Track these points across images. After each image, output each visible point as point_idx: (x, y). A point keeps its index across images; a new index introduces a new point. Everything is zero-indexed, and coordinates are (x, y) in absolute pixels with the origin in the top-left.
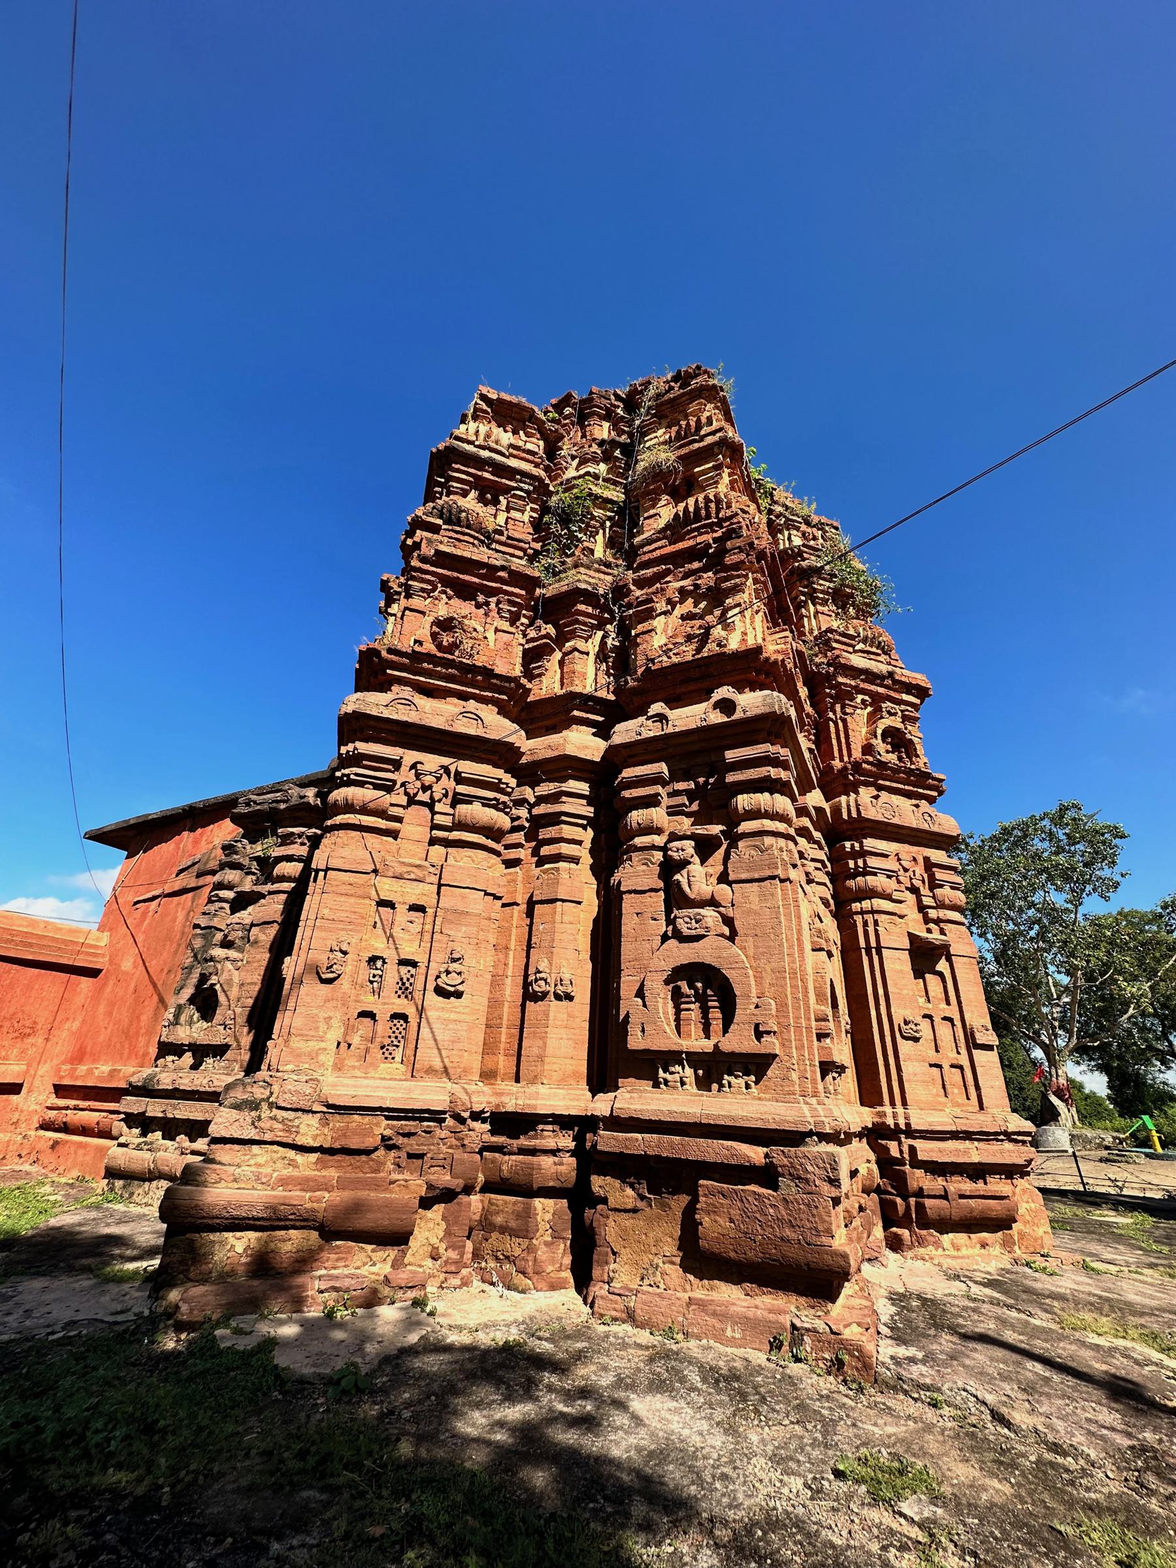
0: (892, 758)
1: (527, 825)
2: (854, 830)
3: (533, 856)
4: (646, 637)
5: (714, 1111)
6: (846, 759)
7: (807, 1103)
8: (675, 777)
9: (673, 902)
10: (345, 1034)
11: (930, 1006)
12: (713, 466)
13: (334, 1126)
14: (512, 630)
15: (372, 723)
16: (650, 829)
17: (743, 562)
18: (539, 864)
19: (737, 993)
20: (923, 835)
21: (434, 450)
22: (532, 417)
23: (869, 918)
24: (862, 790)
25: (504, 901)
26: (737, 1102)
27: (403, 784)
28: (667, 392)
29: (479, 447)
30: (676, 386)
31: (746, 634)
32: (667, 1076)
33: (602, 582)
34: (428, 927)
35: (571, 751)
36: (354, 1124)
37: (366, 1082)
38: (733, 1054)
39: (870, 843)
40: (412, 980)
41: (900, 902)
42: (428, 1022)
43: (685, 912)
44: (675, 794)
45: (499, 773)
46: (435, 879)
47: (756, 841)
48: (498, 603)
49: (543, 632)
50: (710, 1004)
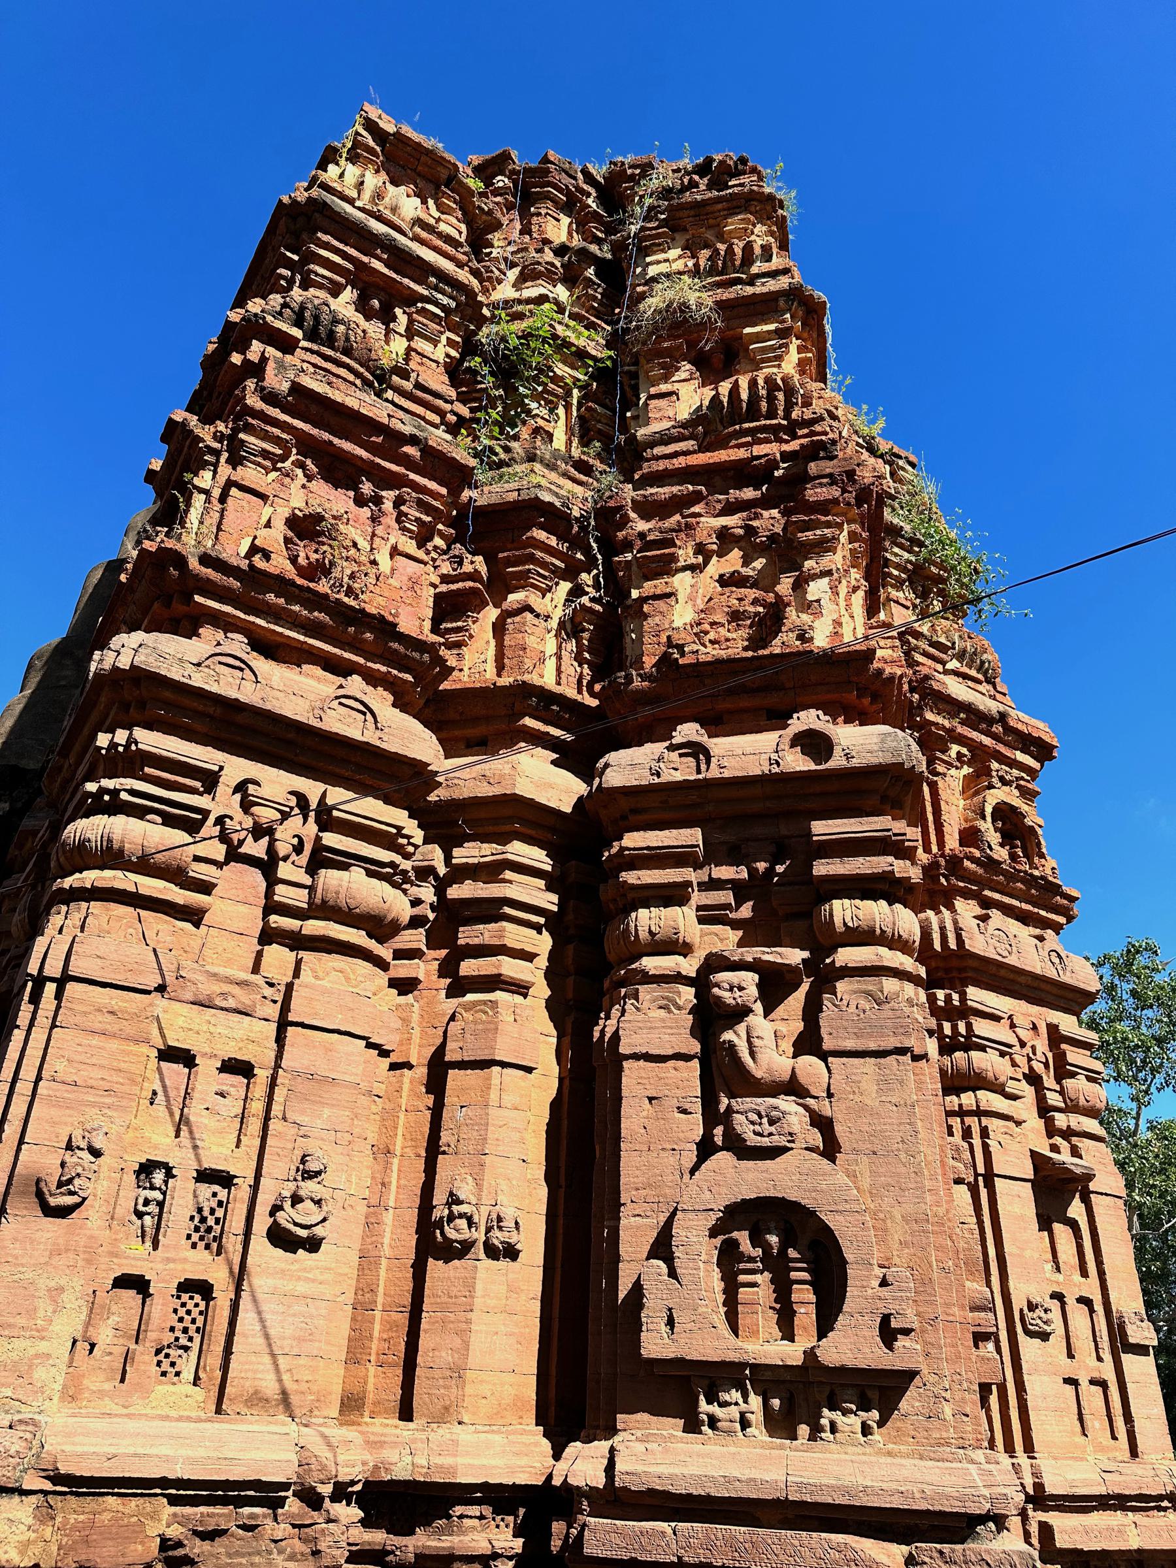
0: (1001, 854)
1: (431, 916)
2: (947, 970)
3: (442, 974)
4: (660, 605)
5: (812, 1476)
6: (935, 849)
7: (972, 1462)
8: (714, 854)
9: (718, 1081)
10: (88, 1324)
11: (1060, 1277)
12: (776, 331)
13: (66, 1520)
14: (420, 554)
15: (168, 694)
16: (675, 946)
17: (835, 501)
18: (452, 992)
19: (849, 1256)
20: (1048, 987)
21: (286, 199)
22: (452, 180)
23: (972, 1121)
24: (959, 904)
25: (394, 1058)
26: (845, 1461)
27: (220, 821)
28: (684, 189)
29: (359, 208)
30: (703, 183)
31: (840, 624)
32: (714, 1409)
33: (575, 496)
34: (257, 1107)
35: (525, 789)
36: (106, 1516)
37: (132, 1425)
38: (842, 1370)
39: (977, 996)
40: (220, 1213)
41: (1014, 1097)
42: (255, 1300)
43: (749, 1103)
44: (713, 885)
45: (399, 817)
46: (273, 1011)
47: (869, 984)
48: (398, 502)
49: (467, 568)
50: (794, 1275)
